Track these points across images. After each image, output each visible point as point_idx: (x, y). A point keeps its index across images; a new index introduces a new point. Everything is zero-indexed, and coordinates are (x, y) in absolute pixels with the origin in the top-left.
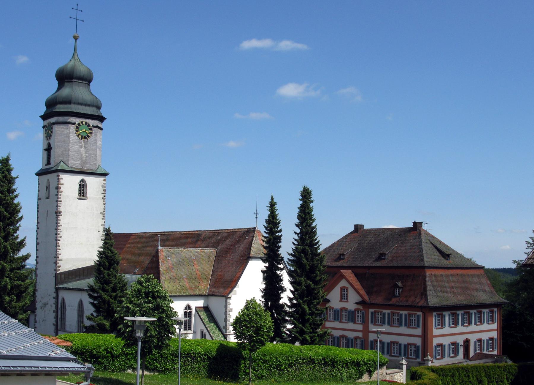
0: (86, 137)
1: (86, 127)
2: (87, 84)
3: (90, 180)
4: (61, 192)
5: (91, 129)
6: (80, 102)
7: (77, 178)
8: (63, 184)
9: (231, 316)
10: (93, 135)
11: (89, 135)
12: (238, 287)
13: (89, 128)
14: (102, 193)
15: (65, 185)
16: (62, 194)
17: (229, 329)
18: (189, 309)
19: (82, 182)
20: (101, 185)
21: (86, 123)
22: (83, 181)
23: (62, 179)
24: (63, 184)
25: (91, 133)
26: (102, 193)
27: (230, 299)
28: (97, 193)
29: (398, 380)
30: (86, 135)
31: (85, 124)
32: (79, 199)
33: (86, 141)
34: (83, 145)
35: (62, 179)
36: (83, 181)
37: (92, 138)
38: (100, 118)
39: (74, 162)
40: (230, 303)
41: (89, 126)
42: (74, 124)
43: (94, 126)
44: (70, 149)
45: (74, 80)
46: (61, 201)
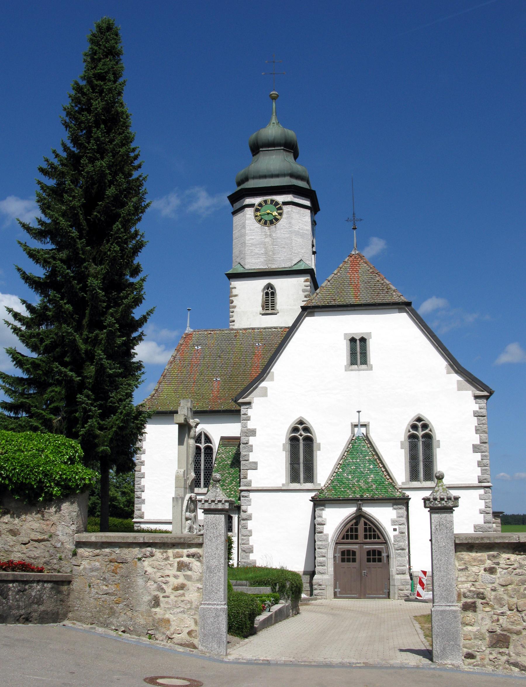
0: (274, 221)
1: (272, 206)
2: (282, 150)
3: (277, 282)
4: (234, 307)
5: (280, 208)
6: (261, 174)
7: (261, 283)
8: (236, 296)
9: (252, 446)
10: (284, 216)
11: (278, 217)
12: (272, 380)
13: (277, 207)
14: (303, 301)
15: (239, 296)
16: (235, 310)
17: (245, 478)
18: (205, 443)
19: (270, 289)
20: (301, 289)
21: (272, 201)
22: (269, 286)
23: (235, 288)
24: (236, 296)
25: (280, 214)
26: (303, 301)
27: (248, 406)
28: (294, 301)
29: (166, 583)
30: (273, 218)
31: (269, 203)
32: (263, 315)
33: (273, 227)
34: (268, 233)
35: (235, 288)
36: (269, 286)
37: (283, 222)
38: (293, 190)
39: (254, 261)
40: (250, 417)
41: (277, 204)
42: (252, 206)
43: (285, 203)
44: (247, 242)
45: (261, 149)
46: (233, 321)
